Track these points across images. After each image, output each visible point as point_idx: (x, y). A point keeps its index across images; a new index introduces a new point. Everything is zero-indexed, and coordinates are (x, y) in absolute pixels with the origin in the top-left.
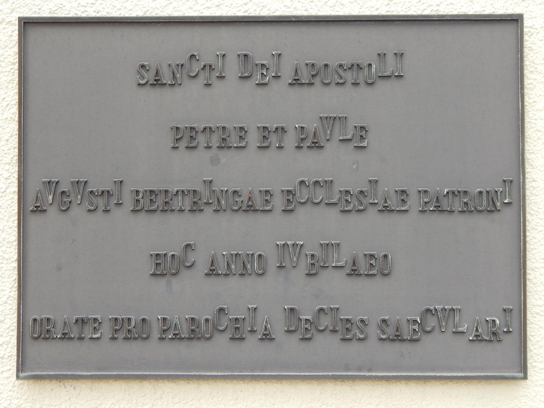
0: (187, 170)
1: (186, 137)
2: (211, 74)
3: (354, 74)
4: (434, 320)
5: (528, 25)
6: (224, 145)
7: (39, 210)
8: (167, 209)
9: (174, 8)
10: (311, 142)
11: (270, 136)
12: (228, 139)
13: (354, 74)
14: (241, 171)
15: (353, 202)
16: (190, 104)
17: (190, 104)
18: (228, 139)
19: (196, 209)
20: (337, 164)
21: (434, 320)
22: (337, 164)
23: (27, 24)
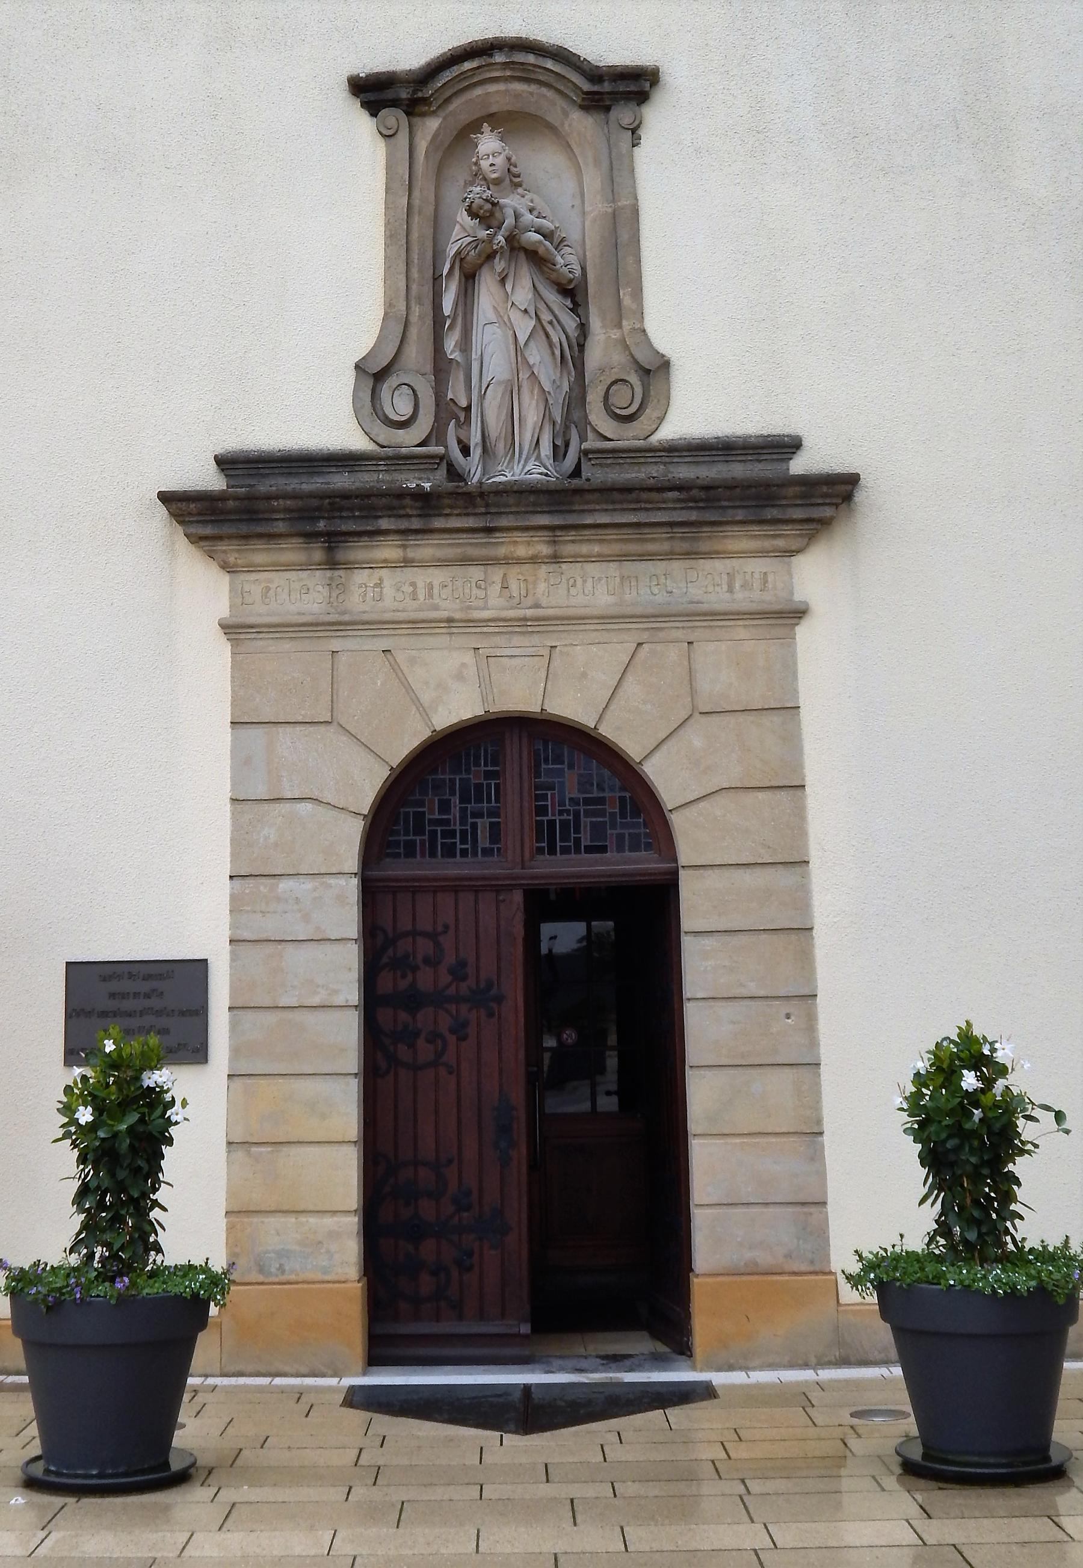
0: (112, 1005)
1: (113, 995)
2: (119, 977)
3: (160, 977)
4: (181, 1047)
5: (342, 881)
6: (123, 998)
7: (71, 1017)
8: (107, 1016)
9: (122, 177)
10: (147, 996)
11: (136, 995)
12: (124, 996)
13: (160, 977)
14: (128, 1005)
15: (159, 1013)
16: (115, 986)
17: (115, 986)
18: (124, 996)
19: (115, 1016)
20: (154, 1003)
21: (181, 1047)
22: (154, 1003)
23: (67, 963)
